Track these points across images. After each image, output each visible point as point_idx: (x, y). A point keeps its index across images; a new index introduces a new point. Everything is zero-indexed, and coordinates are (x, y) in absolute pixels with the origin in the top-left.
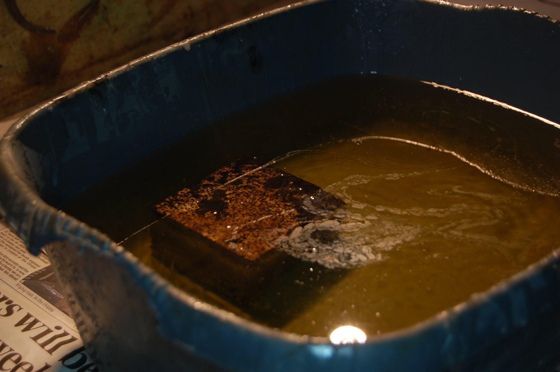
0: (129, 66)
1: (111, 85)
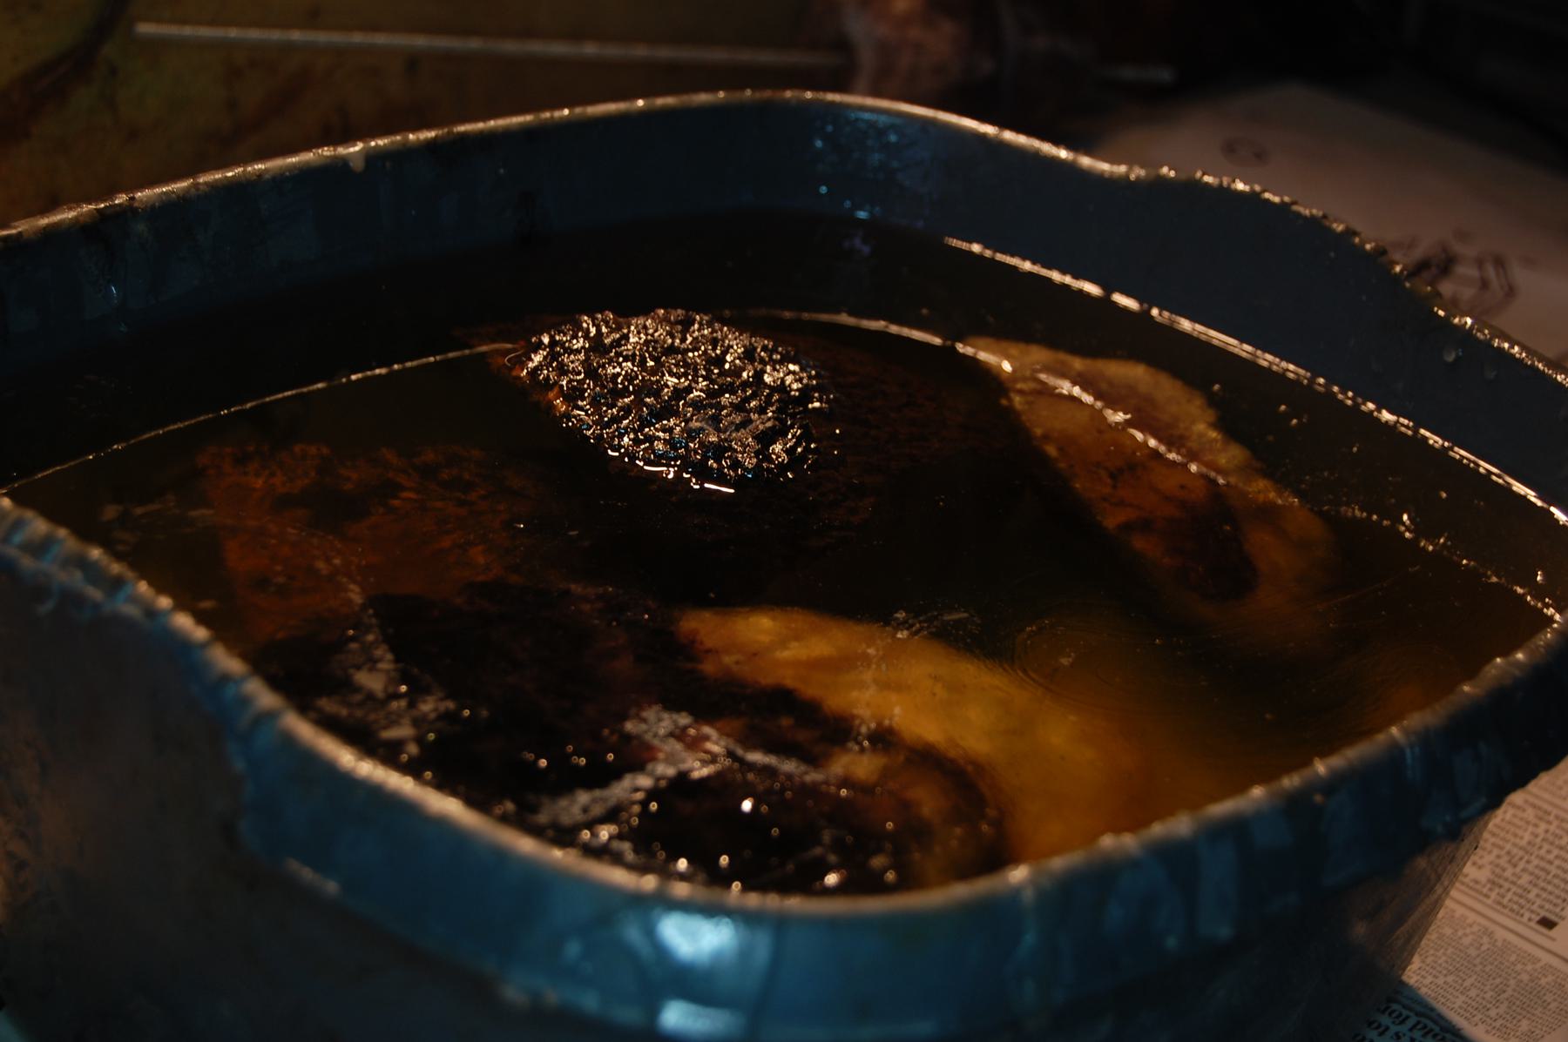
0: (196, 185)
1: (141, 227)
